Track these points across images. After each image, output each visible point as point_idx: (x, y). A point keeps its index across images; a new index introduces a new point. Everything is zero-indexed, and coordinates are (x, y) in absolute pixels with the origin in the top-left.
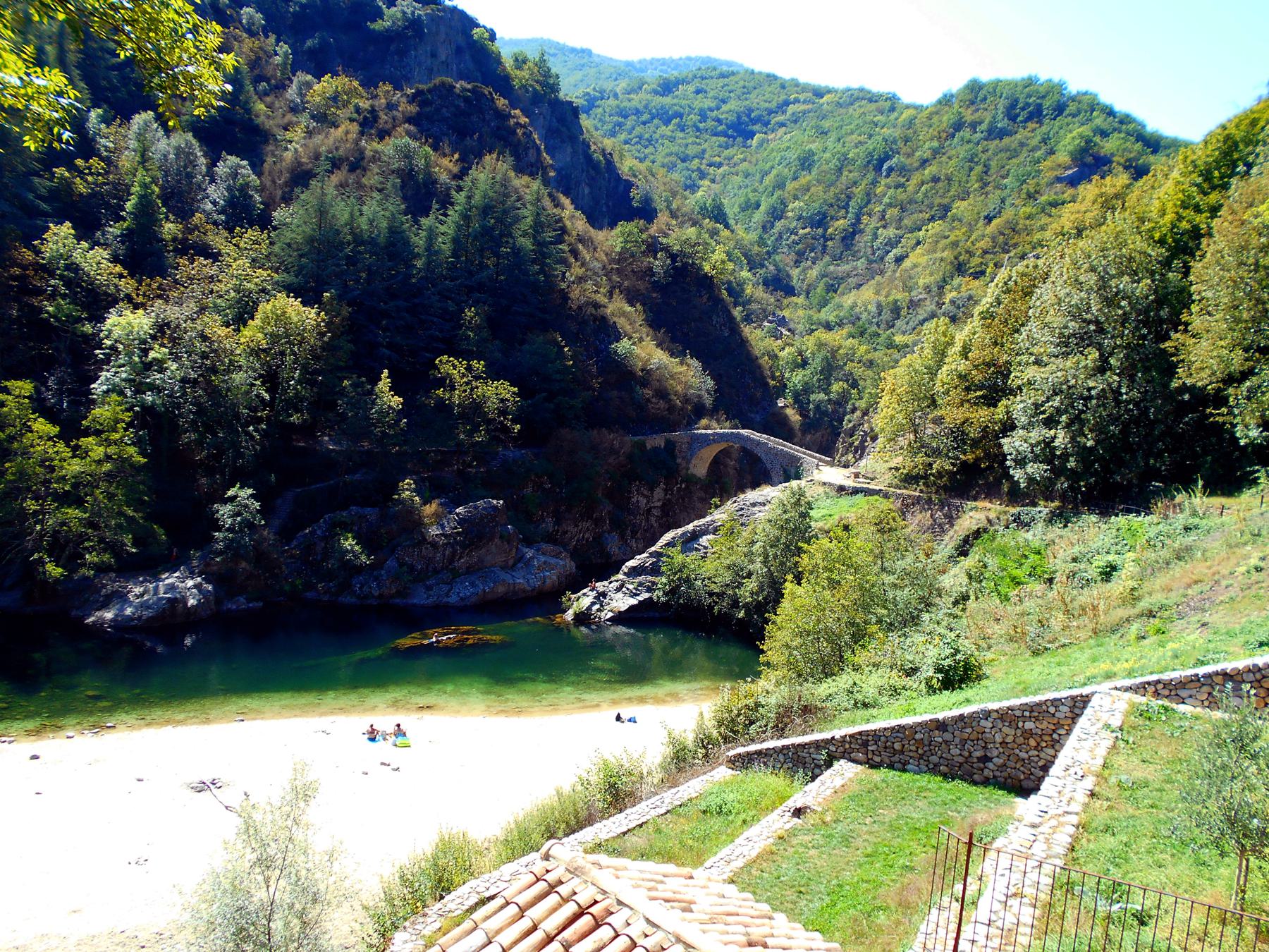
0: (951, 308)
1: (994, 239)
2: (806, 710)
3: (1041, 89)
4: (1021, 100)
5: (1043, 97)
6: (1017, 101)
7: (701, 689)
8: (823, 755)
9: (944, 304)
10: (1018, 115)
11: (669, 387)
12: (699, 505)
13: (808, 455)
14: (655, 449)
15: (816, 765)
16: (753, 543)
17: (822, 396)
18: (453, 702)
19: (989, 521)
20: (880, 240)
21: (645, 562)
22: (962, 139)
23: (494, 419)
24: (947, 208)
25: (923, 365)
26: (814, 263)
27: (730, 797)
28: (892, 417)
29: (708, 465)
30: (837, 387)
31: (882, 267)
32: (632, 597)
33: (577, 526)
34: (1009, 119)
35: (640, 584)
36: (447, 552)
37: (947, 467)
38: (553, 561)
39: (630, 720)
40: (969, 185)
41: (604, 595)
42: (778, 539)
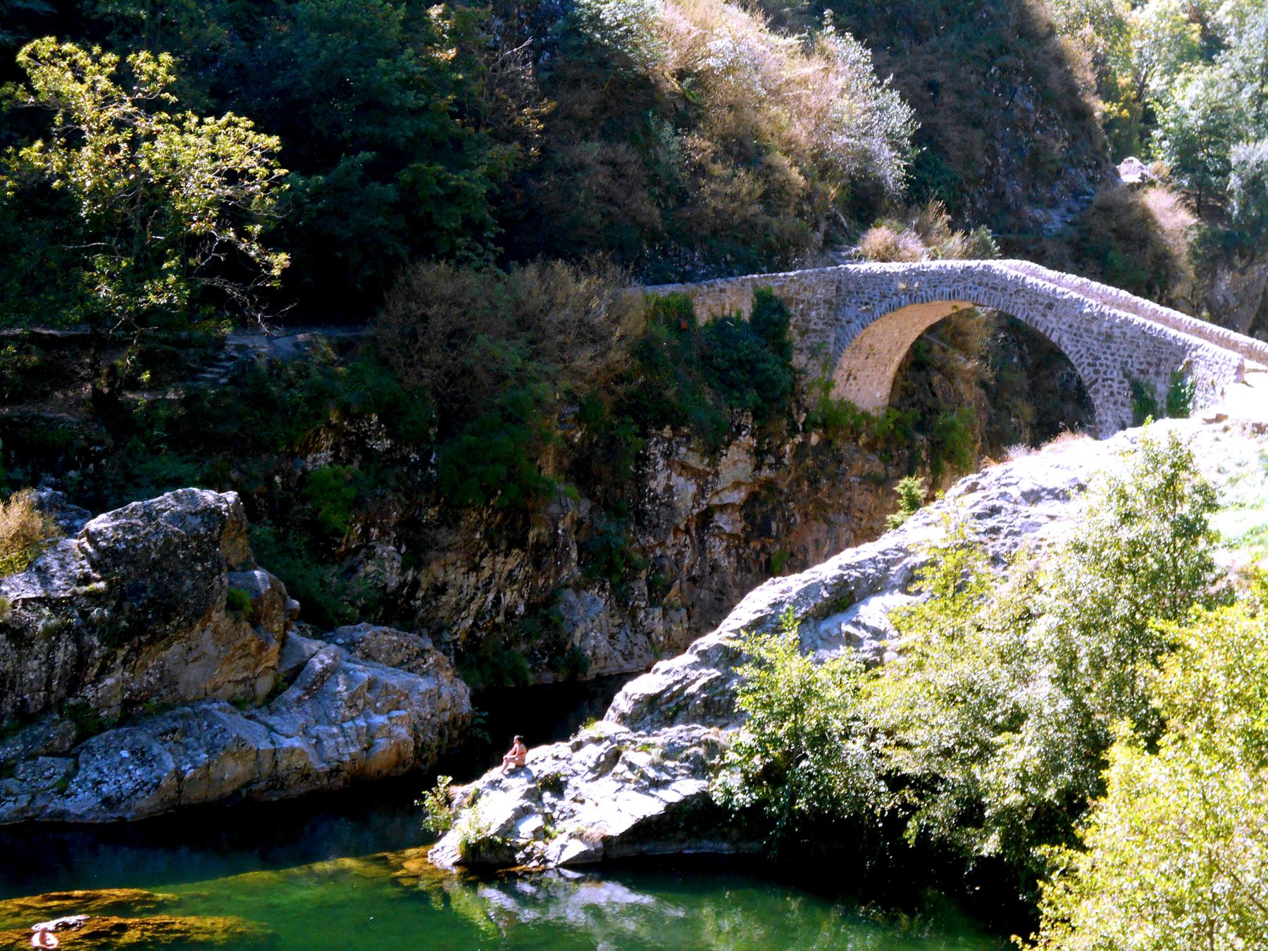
11: (765, 126)
12: (863, 498)
13: (1210, 337)
14: (720, 326)
16: (1028, 617)
21: (685, 682)
29: (892, 370)
32: (644, 790)
33: (476, 568)
35: (671, 752)
36: (60, 656)
38: (397, 679)
42: (1105, 606)
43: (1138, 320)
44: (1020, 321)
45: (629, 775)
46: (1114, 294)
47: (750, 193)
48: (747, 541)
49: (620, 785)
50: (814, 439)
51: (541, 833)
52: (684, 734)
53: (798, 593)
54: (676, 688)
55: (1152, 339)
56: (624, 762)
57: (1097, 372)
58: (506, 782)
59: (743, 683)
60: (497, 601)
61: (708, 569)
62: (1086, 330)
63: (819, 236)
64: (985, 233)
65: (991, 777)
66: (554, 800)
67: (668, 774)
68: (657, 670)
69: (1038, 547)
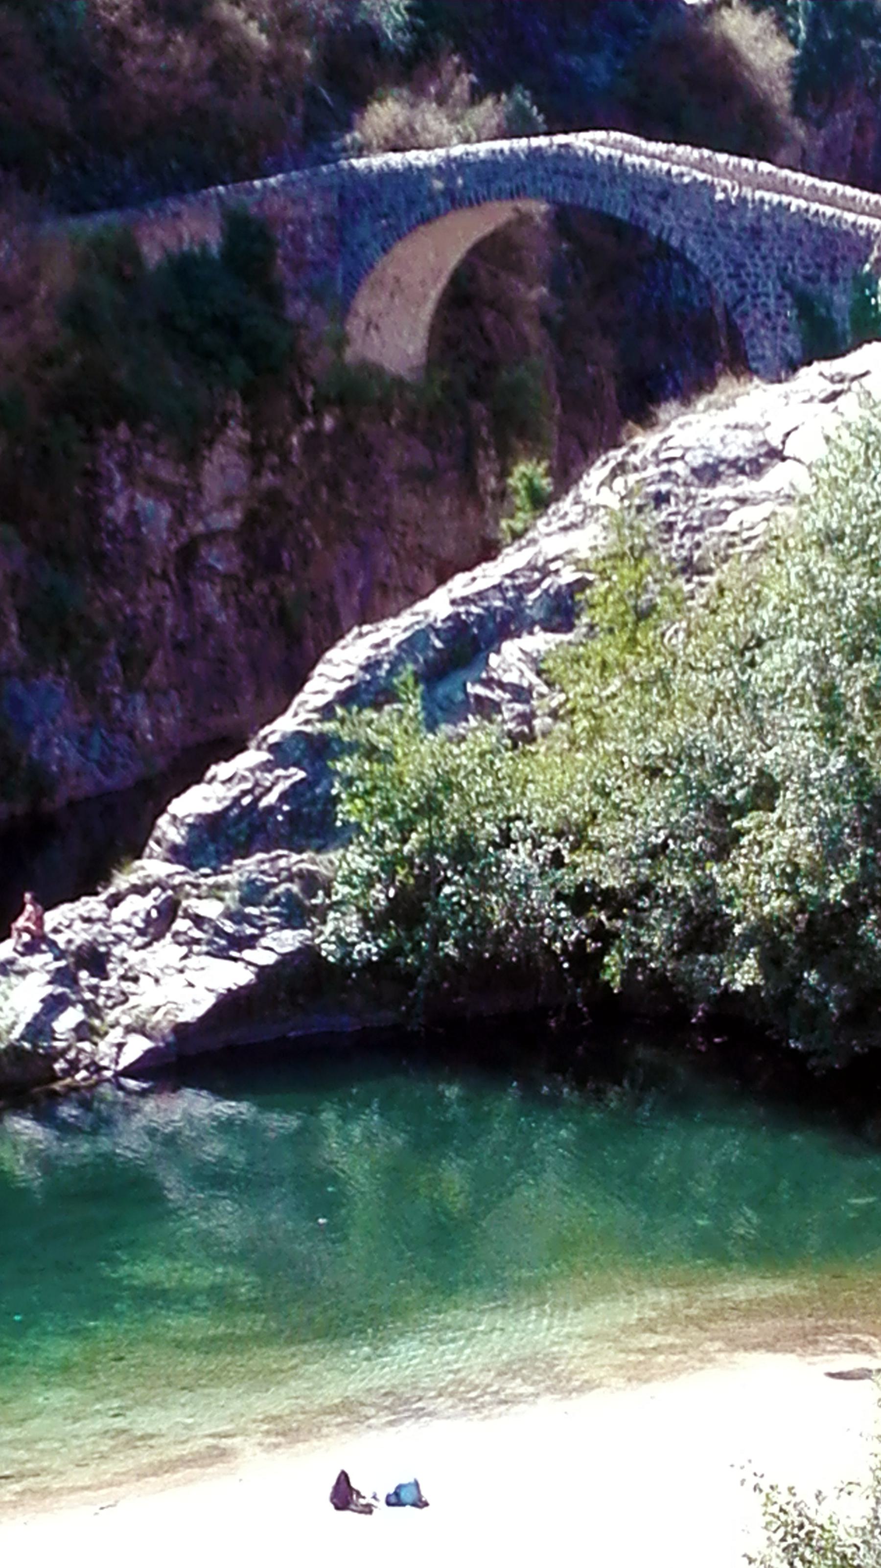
21: (259, 791)
29: (430, 307)
32: (220, 954)
43: (796, 203)
44: (620, 221)
45: (196, 934)
46: (751, 168)
47: (194, 65)
48: (249, 583)
49: (184, 950)
50: (328, 423)
51: (85, 1030)
52: (266, 866)
53: (399, 646)
54: (246, 801)
55: (821, 230)
56: (187, 915)
57: (742, 285)
58: (24, 962)
59: (349, 782)
61: (199, 629)
62: (720, 225)
63: (296, 122)
64: (522, 97)
65: (737, 877)
66: (94, 981)
67: (253, 925)
68: (213, 778)
69: (731, 545)
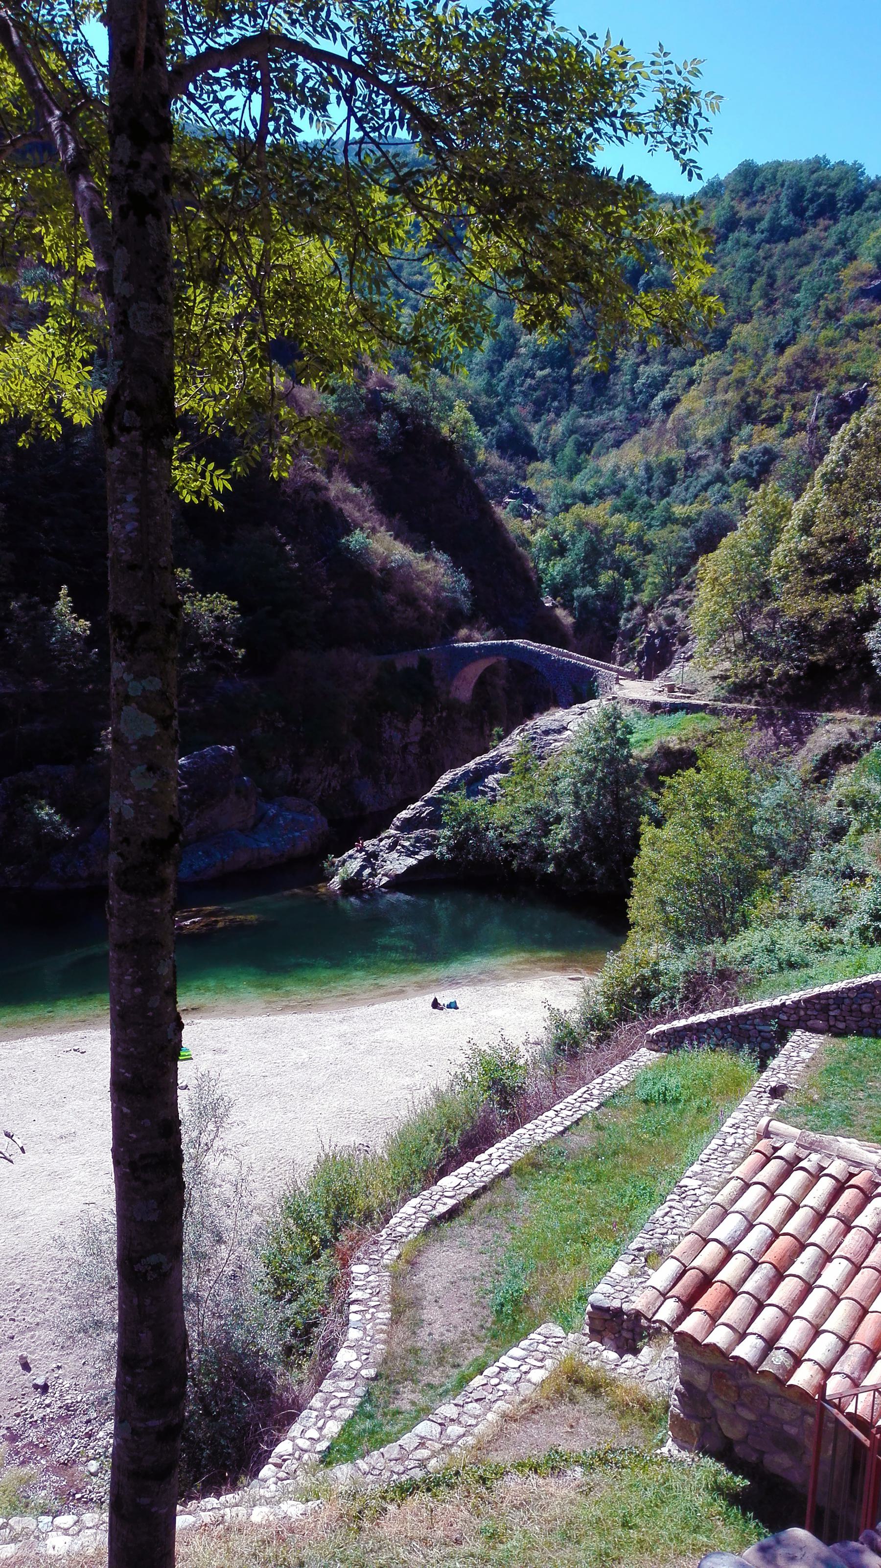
0: (742, 466)
1: (789, 372)
2: (723, 976)
3: (832, 174)
4: (809, 189)
5: (836, 185)
6: (803, 190)
7: (520, 963)
8: (774, 1026)
9: (731, 461)
10: (805, 209)
13: (601, 666)
15: (763, 1038)
17: (588, 590)
18: (223, 1000)
19: (852, 735)
20: (642, 381)
21: (421, 812)
22: (738, 241)
23: (210, 644)
24: (724, 335)
25: (749, 545)
26: (558, 415)
27: (673, 1082)
28: (715, 614)
29: (473, 685)
30: (606, 577)
31: (646, 416)
32: (409, 856)
33: (321, 772)
34: (795, 215)
35: (418, 839)
37: (791, 672)
39: (449, 1006)
40: (751, 303)
41: (374, 855)
42: (591, 774)
43: (574, 661)
50: (444, 714)
59: (445, 811)
60: (329, 785)
64: (501, 629)
